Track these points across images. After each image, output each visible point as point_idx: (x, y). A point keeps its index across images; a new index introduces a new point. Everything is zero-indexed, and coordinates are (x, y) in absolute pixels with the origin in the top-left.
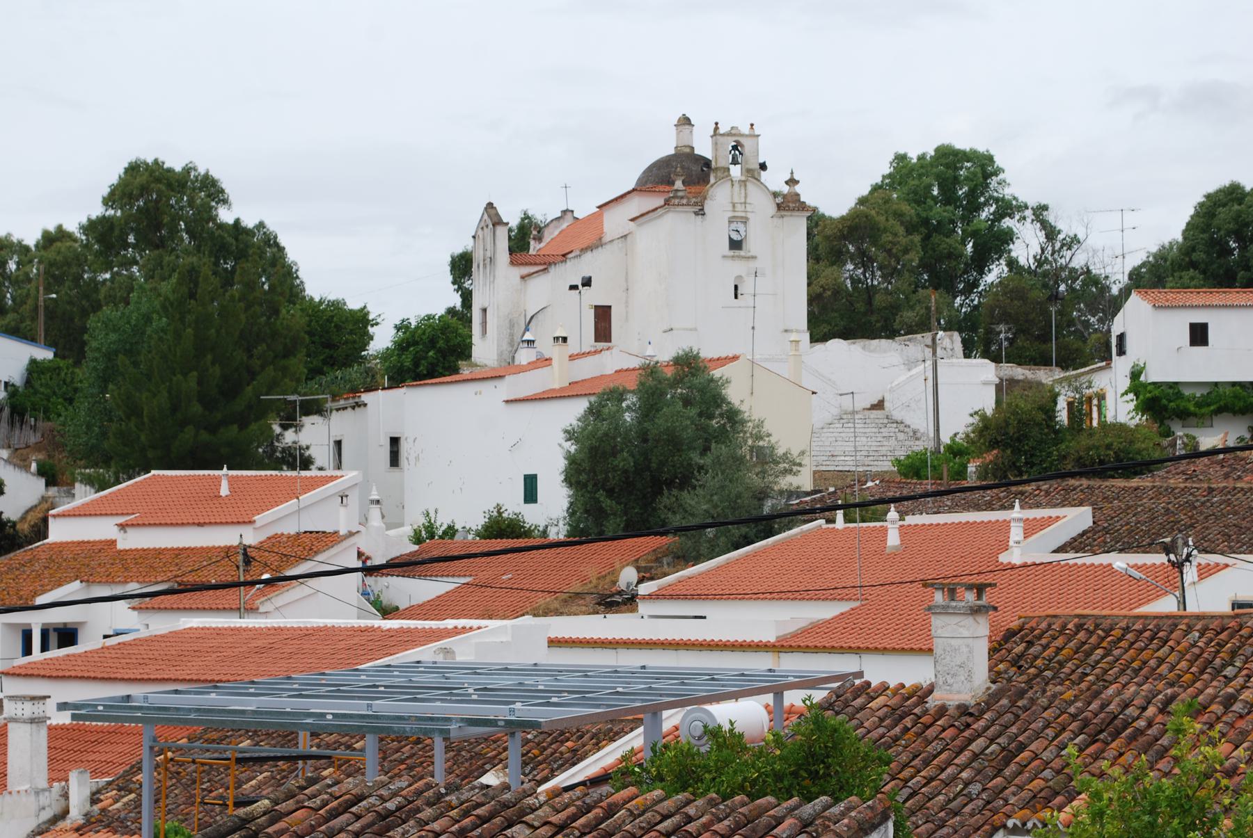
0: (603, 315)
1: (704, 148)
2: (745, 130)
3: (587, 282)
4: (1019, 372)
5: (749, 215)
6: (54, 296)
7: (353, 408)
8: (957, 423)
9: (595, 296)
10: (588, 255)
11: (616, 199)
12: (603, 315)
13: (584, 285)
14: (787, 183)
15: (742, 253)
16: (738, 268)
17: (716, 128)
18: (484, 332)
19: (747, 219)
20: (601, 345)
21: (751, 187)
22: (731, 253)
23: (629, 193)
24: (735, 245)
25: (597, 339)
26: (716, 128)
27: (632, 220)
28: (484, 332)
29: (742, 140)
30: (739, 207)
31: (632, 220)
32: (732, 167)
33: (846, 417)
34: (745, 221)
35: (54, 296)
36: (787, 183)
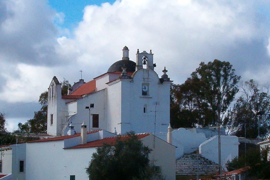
0: (96, 118)
1: (133, 58)
2: (149, 52)
3: (92, 106)
4: (247, 141)
5: (149, 82)
6: (259, 164)
7: (7, 150)
8: (69, 135)
9: (94, 111)
10: (90, 96)
11: (101, 76)
12: (96, 118)
13: (91, 107)
14: (163, 71)
15: (147, 96)
16: (144, 101)
17: (138, 51)
18: (52, 123)
19: (149, 84)
20: (95, 129)
21: (150, 72)
22: (143, 96)
23: (105, 74)
24: (144, 93)
25: (93, 127)
26: (138, 51)
27: (106, 84)
28: (52, 123)
29: (147, 56)
30: (146, 80)
31: (106, 84)
32: (143, 65)
33: (186, 155)
34: (148, 85)
35: (259, 164)
36: (163, 71)
